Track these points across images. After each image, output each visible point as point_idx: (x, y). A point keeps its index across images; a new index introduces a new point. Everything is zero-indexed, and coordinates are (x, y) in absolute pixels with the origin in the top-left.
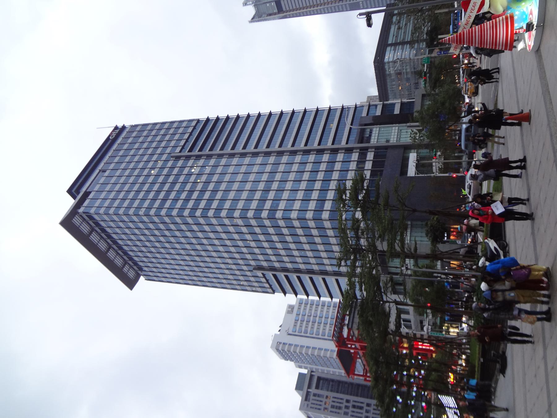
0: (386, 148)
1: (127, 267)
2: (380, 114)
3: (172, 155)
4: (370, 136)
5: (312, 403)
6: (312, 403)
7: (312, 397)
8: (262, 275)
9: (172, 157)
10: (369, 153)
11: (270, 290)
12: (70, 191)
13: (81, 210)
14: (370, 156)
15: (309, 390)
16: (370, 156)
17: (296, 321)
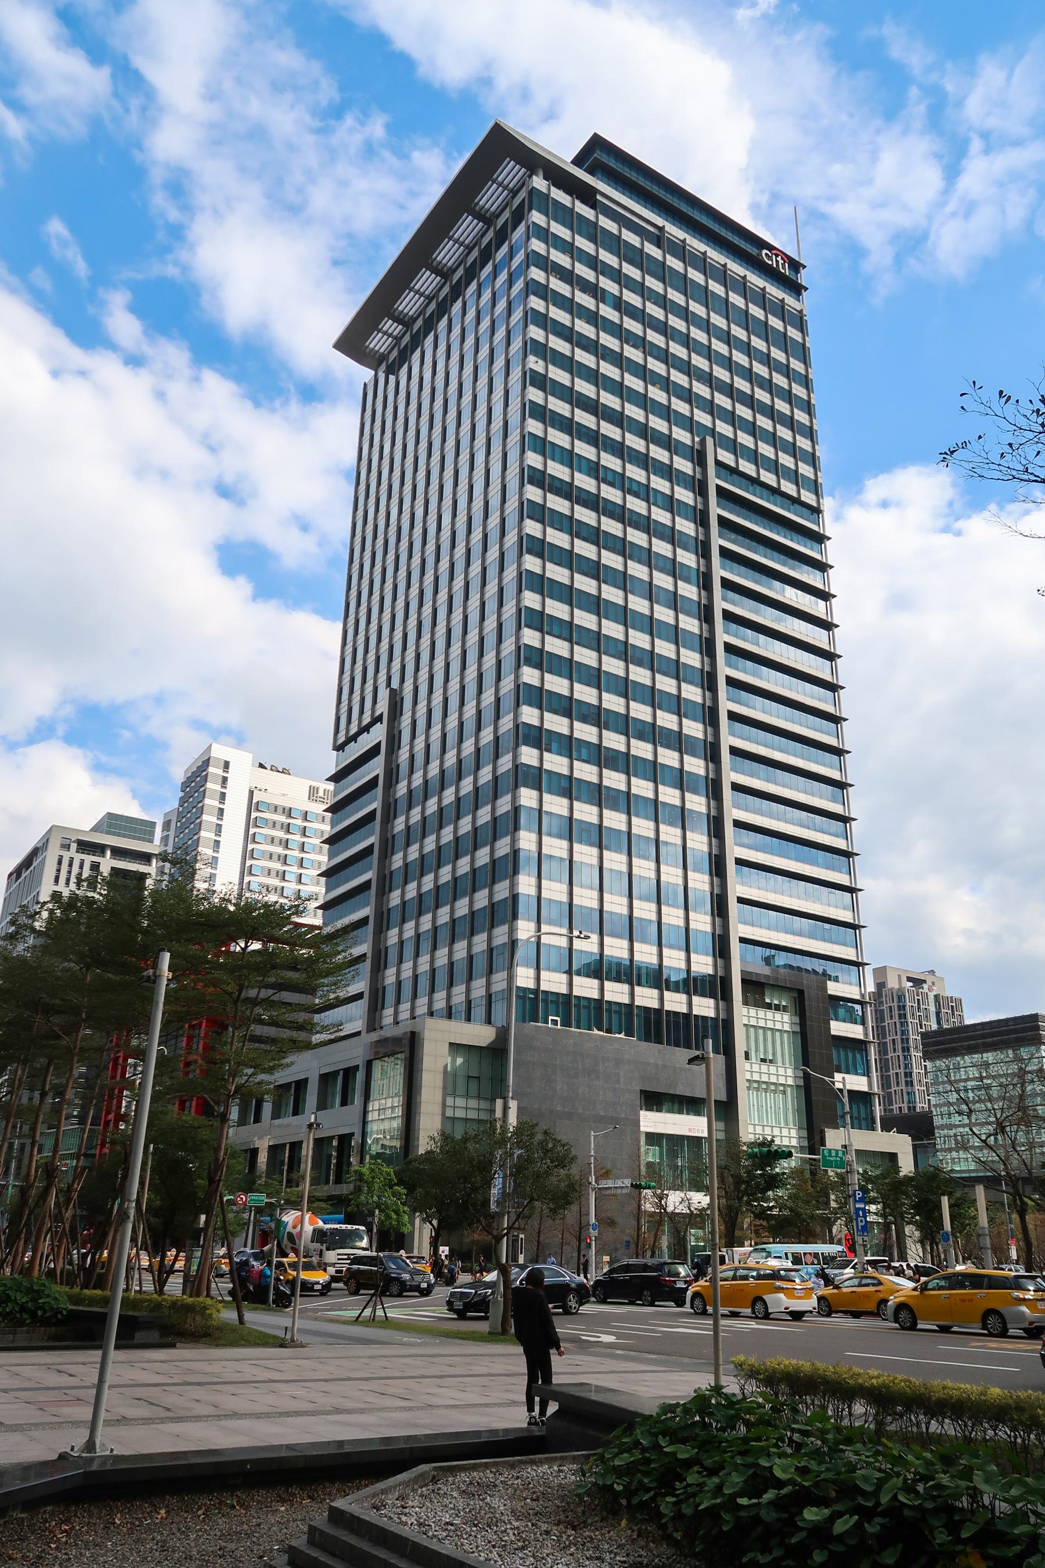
0: (728, 1050)
1: (396, 329)
2: (833, 1033)
3: (709, 441)
4: (769, 1006)
5: (71, 860)
6: (71, 860)
7: (89, 859)
8: (377, 713)
9: (703, 442)
10: (711, 1002)
11: (342, 739)
12: (597, 143)
13: (539, 183)
14: (705, 1007)
15: (108, 853)
16: (705, 1007)
17: (289, 812)
